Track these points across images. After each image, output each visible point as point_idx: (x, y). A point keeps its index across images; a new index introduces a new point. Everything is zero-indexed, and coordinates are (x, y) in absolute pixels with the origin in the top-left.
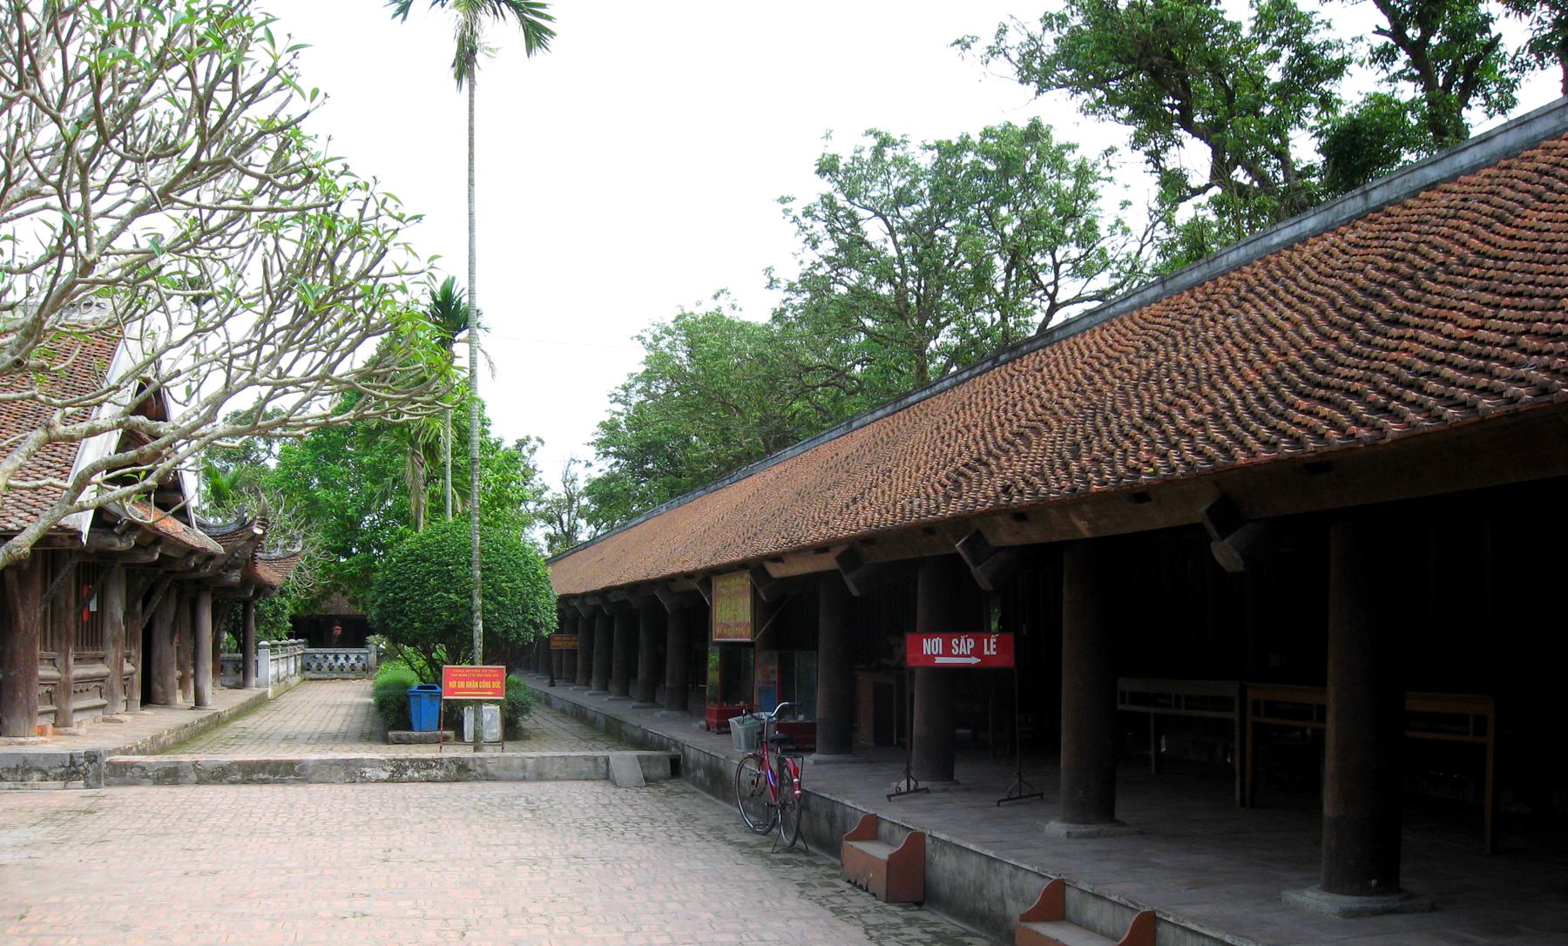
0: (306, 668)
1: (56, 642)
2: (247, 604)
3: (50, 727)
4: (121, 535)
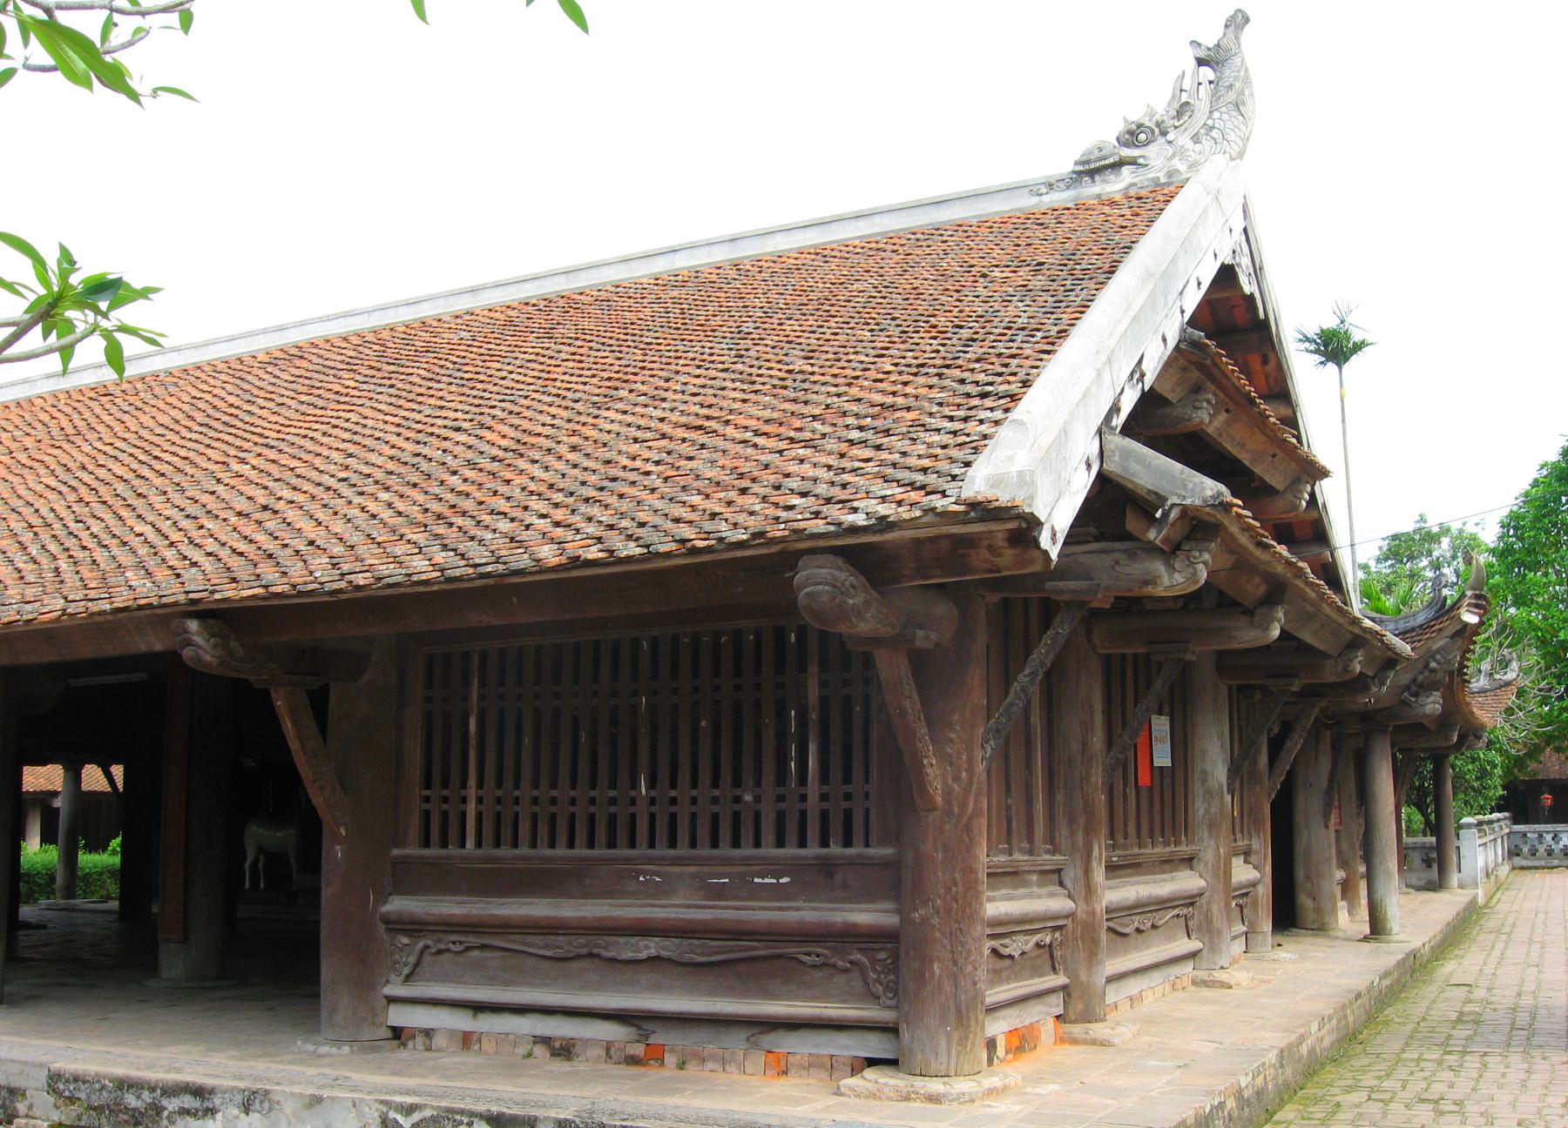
0: (1514, 853)
1: (1063, 832)
2: (1439, 759)
3: (1048, 1028)
4: (1171, 552)
